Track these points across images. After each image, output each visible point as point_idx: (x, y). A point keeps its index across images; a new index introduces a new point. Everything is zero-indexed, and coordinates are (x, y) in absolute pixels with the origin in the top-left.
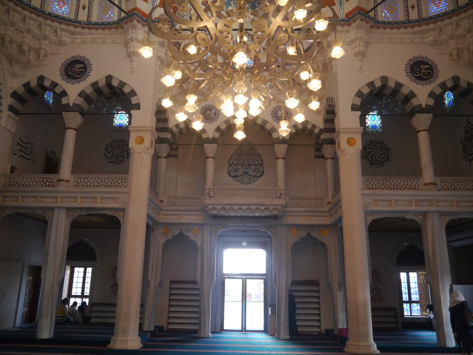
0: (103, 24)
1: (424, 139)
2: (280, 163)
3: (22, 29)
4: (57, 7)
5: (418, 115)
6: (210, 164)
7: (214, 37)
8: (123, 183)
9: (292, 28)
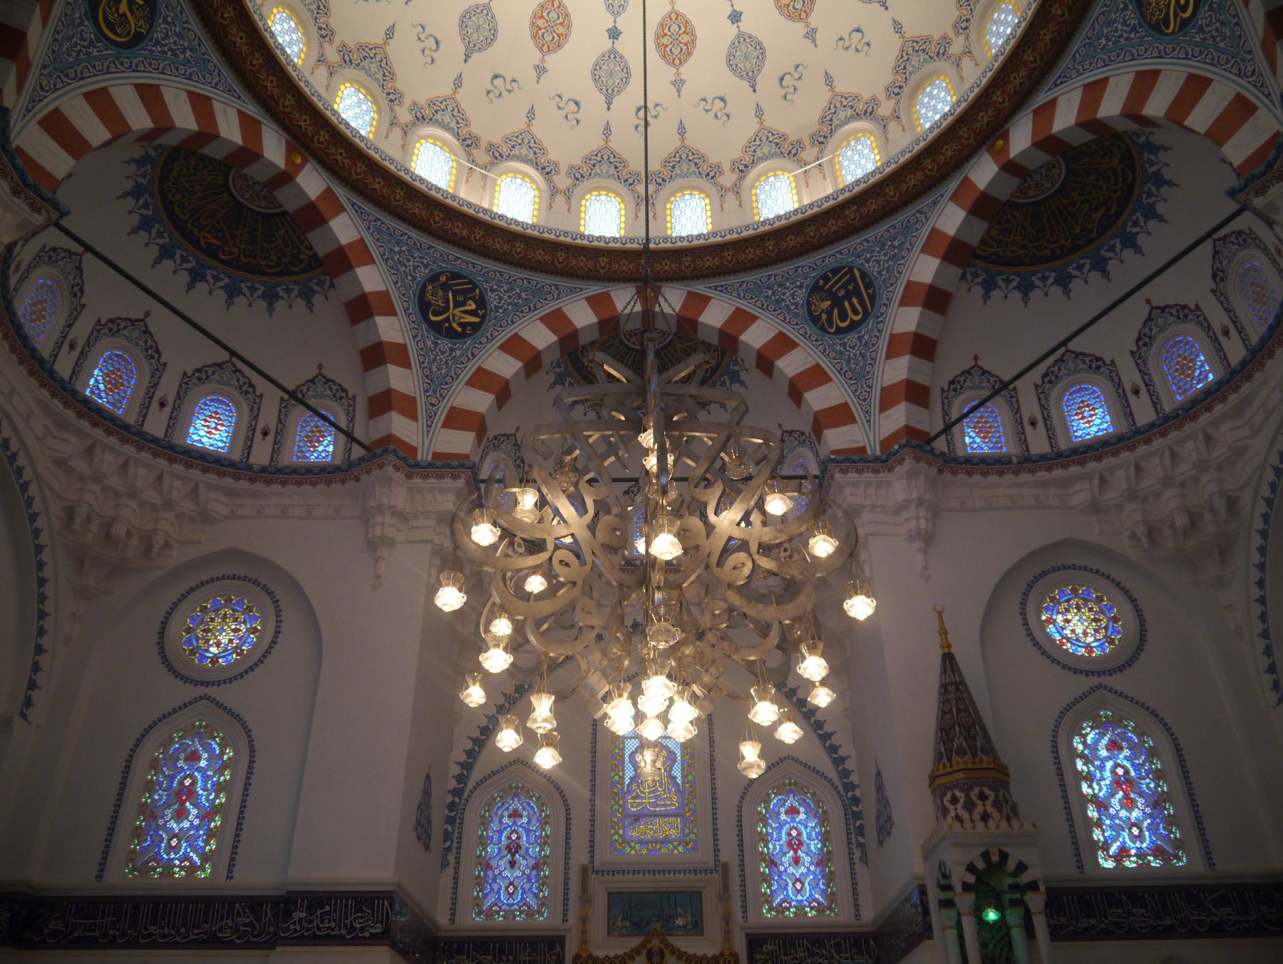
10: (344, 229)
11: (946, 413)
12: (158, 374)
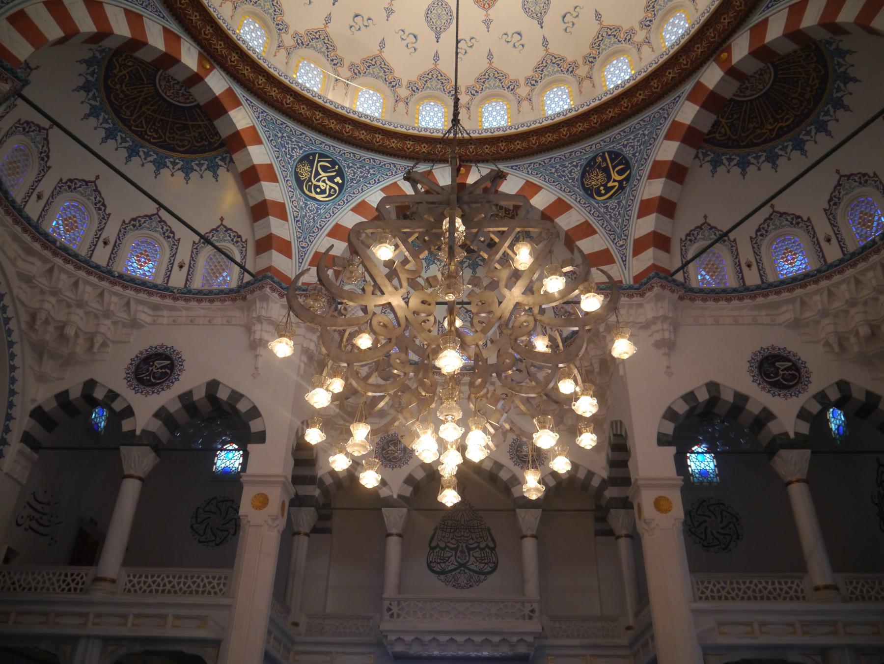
0: (211, 292)
1: (799, 495)
2: (529, 546)
3: (69, 300)
4: (135, 265)
5: (783, 452)
6: (394, 547)
7: (403, 321)
8: (222, 586)
9: (540, 306)
12: (734, 248)
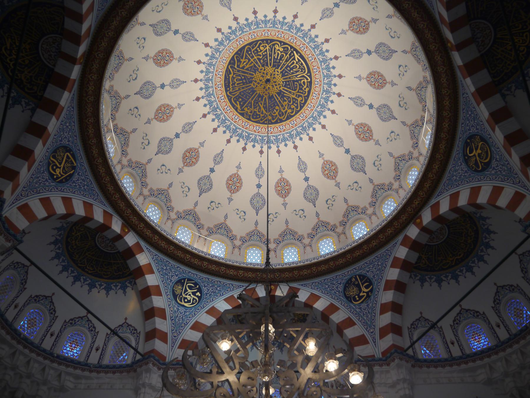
0: (114, 367)
9: (324, 381)
10: (143, 259)
11: (411, 338)
